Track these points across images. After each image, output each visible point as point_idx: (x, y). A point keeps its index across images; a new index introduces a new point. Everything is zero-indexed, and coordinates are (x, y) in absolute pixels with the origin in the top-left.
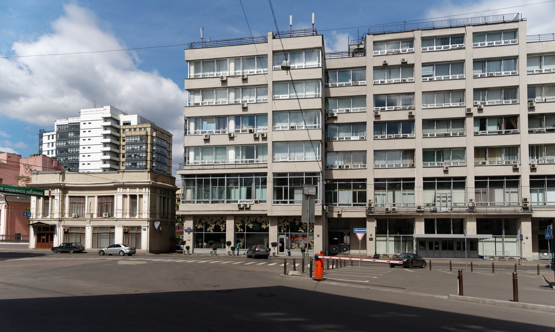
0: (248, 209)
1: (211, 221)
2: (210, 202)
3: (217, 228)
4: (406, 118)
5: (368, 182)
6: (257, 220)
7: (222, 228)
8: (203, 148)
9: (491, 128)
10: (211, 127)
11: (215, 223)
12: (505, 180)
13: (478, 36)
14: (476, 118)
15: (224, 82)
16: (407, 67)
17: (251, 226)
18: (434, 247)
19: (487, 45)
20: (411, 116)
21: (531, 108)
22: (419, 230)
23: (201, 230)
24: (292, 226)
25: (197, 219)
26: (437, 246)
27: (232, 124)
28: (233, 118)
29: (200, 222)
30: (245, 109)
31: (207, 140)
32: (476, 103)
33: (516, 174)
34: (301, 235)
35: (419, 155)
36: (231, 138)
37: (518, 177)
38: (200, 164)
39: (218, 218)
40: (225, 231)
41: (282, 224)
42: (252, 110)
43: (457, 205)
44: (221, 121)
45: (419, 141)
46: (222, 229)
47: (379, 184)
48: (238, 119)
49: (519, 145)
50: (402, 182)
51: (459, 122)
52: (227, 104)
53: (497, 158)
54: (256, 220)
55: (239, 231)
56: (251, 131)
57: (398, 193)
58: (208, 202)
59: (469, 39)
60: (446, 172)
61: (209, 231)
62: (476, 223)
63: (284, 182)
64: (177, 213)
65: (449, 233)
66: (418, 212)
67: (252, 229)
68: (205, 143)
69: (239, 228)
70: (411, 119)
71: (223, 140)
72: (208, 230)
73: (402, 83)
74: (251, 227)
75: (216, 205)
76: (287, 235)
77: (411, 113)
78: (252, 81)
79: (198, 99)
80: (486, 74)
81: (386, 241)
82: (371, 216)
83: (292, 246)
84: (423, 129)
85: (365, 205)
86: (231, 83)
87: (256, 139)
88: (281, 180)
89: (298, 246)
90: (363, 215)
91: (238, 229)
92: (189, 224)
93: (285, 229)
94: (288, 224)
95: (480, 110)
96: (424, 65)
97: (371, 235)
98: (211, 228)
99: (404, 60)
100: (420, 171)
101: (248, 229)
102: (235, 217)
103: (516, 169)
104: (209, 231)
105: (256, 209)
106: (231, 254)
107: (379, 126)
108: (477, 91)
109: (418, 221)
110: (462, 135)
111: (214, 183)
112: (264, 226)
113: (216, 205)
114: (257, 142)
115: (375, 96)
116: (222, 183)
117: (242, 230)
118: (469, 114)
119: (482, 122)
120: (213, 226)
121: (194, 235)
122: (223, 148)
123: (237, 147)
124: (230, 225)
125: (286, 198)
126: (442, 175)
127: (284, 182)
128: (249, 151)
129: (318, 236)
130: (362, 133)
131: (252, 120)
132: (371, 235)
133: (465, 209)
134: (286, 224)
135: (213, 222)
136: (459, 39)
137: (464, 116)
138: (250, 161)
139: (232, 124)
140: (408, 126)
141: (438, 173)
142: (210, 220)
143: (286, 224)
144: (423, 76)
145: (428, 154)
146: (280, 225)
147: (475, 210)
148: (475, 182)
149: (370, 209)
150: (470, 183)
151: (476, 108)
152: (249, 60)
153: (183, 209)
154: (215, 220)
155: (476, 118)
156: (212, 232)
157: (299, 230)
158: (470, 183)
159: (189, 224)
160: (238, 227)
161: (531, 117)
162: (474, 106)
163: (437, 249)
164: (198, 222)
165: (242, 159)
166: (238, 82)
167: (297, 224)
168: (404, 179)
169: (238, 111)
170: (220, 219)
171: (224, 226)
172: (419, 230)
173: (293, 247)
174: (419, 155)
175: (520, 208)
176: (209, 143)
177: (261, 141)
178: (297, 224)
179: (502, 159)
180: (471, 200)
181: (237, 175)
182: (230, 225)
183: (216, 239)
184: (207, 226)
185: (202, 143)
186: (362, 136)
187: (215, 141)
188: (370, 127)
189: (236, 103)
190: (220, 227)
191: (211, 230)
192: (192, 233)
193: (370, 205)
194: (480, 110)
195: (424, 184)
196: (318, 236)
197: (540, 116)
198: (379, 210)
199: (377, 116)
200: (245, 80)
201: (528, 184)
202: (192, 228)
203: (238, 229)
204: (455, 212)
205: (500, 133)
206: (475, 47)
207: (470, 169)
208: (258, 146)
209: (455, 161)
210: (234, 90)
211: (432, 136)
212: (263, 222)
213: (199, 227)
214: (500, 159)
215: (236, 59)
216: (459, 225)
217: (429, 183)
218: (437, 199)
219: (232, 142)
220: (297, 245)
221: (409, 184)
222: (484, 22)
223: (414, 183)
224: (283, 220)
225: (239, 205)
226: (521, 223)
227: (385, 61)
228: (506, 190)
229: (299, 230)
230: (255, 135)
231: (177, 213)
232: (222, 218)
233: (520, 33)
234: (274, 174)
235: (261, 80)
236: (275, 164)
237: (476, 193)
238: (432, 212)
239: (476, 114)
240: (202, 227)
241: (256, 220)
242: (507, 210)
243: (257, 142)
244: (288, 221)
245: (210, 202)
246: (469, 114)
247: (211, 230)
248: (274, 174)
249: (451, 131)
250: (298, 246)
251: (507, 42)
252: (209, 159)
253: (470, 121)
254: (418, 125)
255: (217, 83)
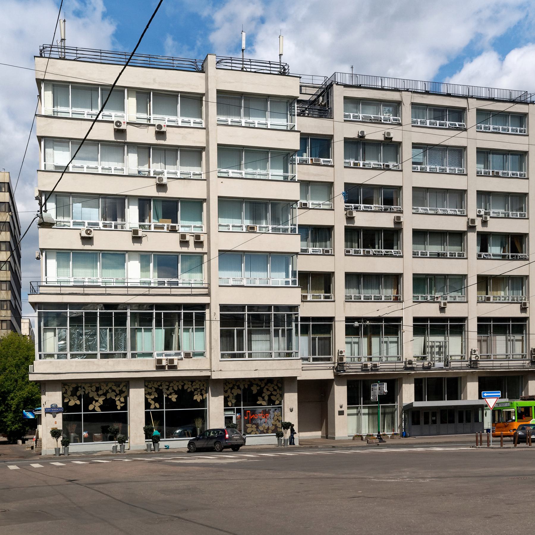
0: (173, 367)
1: (98, 389)
2: (99, 356)
3: (109, 404)
4: (391, 225)
5: (404, 322)
6: (186, 387)
7: (118, 403)
8: (76, 253)
9: (495, 250)
10: (93, 214)
11: (105, 394)
12: (429, 323)
13: (483, 115)
14: (480, 234)
15: (120, 132)
16: (391, 146)
17: (174, 398)
18: (430, 421)
19: (491, 130)
20: (398, 222)
21: (350, 219)
22: (408, 394)
23: (77, 408)
24: (251, 395)
25: (70, 387)
26: (434, 418)
27: (132, 212)
28: (137, 202)
29: (74, 394)
30: (161, 187)
31: (87, 240)
32: (480, 212)
33: (523, 315)
34: (261, 410)
35: (408, 284)
36: (137, 239)
37: (526, 319)
38: (72, 284)
39: (110, 385)
40: (125, 408)
41: (229, 393)
42: (175, 190)
43: (497, 357)
44: (113, 207)
45: (407, 263)
46: (119, 405)
47: (353, 327)
48: (144, 203)
49: (527, 277)
50: (511, 323)
51: (458, 237)
52: (127, 175)
53: (499, 292)
54: (183, 386)
55: (152, 406)
56: (173, 230)
57: (375, 341)
58: (94, 356)
59: (471, 117)
60: (442, 309)
61: (94, 410)
62: (477, 383)
63: (238, 321)
64: (32, 378)
65: (442, 399)
66: (406, 368)
67: (177, 405)
68: (83, 244)
69: (152, 402)
70: (397, 227)
71: (120, 241)
72: (91, 407)
73: (384, 169)
74: (174, 400)
75: (110, 361)
76: (239, 411)
77: (399, 218)
78: (174, 138)
79: (61, 157)
80: (491, 171)
81: (357, 414)
82: (340, 376)
83: (246, 428)
84: (413, 244)
85: (329, 359)
86: (134, 135)
87: (184, 243)
88: (231, 317)
89: (257, 428)
90: (329, 375)
91: (150, 404)
92: (52, 398)
93: (234, 401)
94: (240, 392)
95: (485, 223)
96: (415, 146)
97: (341, 407)
98: (97, 404)
99: (389, 134)
100: (409, 309)
101: (170, 404)
102: (146, 382)
103: (524, 309)
104: (94, 410)
105: (187, 368)
106: (61, 452)
107: (353, 234)
108: (483, 196)
109: (405, 383)
110: (461, 256)
111: (106, 320)
112: (198, 398)
113: (111, 361)
114: (185, 249)
115: (347, 186)
116: (121, 320)
117: (157, 405)
118: (471, 227)
119: (484, 240)
120: (101, 400)
121: (65, 419)
122: (117, 258)
123: (144, 257)
124: (137, 398)
125: (240, 348)
126: (437, 314)
127: (238, 321)
128: (167, 263)
129: (291, 410)
130: (324, 243)
131: (169, 209)
132: (341, 407)
133: (464, 364)
134: (236, 392)
135: (100, 392)
136: (459, 114)
137: (465, 229)
138: (169, 283)
139: (132, 212)
140: (390, 238)
141: (431, 310)
142: (94, 389)
143: (236, 392)
144: (414, 163)
145: (422, 282)
146: (227, 395)
147: (478, 365)
148: (478, 325)
149: (340, 366)
150: (472, 326)
151: (480, 219)
152: (165, 98)
153: (41, 369)
154: (104, 388)
155: (480, 234)
156: (99, 411)
157: (258, 403)
158: (472, 326)
159: (52, 398)
160: (149, 400)
161: (348, 230)
162: (478, 216)
163: (434, 422)
164: (69, 393)
165: (153, 277)
166: (147, 136)
167: (255, 392)
168: (496, 319)
169: (149, 189)
170: (114, 388)
171: (122, 400)
172: (408, 394)
173: (249, 430)
174: (408, 284)
175: (527, 362)
176: (92, 244)
177: (192, 248)
178: (255, 392)
179: (505, 294)
180: (475, 351)
181: (151, 306)
182: (137, 398)
183: (110, 423)
184: (89, 400)
185: (78, 245)
186: (328, 249)
187: (104, 240)
188: (339, 235)
189: (140, 175)
190: (114, 401)
191: (96, 407)
192: (60, 416)
193: (341, 359)
194: (485, 223)
195: (479, 326)
196: (291, 410)
197: (358, 230)
198: (353, 368)
199: (350, 219)
200: (160, 134)
201: (476, 329)
202: (60, 405)
203: (150, 404)
204: (454, 368)
205: (504, 258)
206: (414, 125)
207: (471, 308)
208: (187, 256)
209: (453, 294)
210: (135, 150)
211: (424, 255)
212: (195, 390)
213: (71, 404)
214: (502, 293)
215: (143, 95)
216: (452, 386)
217: (421, 326)
218: (428, 350)
219: (137, 247)
220: (254, 426)
221: (392, 326)
222: (488, 96)
223: (221, 326)
224: (231, 386)
225: (159, 361)
226: (527, 383)
227: (362, 132)
228: (385, 339)
229: (258, 403)
230: (183, 236)
231: (32, 378)
232: (123, 385)
233: (532, 120)
234: (223, 307)
235: (193, 138)
236: (231, 288)
237: (479, 341)
238: (424, 368)
239: (480, 228)
240: (78, 402)
241: (183, 386)
242: (515, 365)
243: (185, 249)
244: (239, 388)
245: (99, 356)
246: (471, 227)
247: (96, 407)
248: (223, 307)
249: (449, 249)
250: (257, 428)
251: (433, 124)
252: (85, 274)
253: (472, 239)
254: (407, 236)
255: (105, 132)
